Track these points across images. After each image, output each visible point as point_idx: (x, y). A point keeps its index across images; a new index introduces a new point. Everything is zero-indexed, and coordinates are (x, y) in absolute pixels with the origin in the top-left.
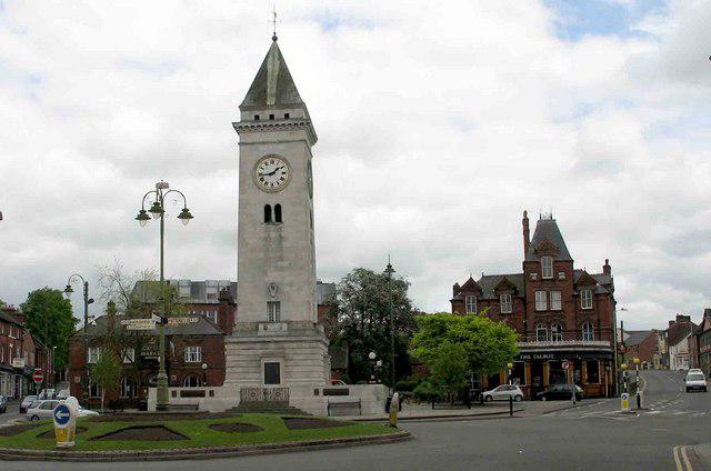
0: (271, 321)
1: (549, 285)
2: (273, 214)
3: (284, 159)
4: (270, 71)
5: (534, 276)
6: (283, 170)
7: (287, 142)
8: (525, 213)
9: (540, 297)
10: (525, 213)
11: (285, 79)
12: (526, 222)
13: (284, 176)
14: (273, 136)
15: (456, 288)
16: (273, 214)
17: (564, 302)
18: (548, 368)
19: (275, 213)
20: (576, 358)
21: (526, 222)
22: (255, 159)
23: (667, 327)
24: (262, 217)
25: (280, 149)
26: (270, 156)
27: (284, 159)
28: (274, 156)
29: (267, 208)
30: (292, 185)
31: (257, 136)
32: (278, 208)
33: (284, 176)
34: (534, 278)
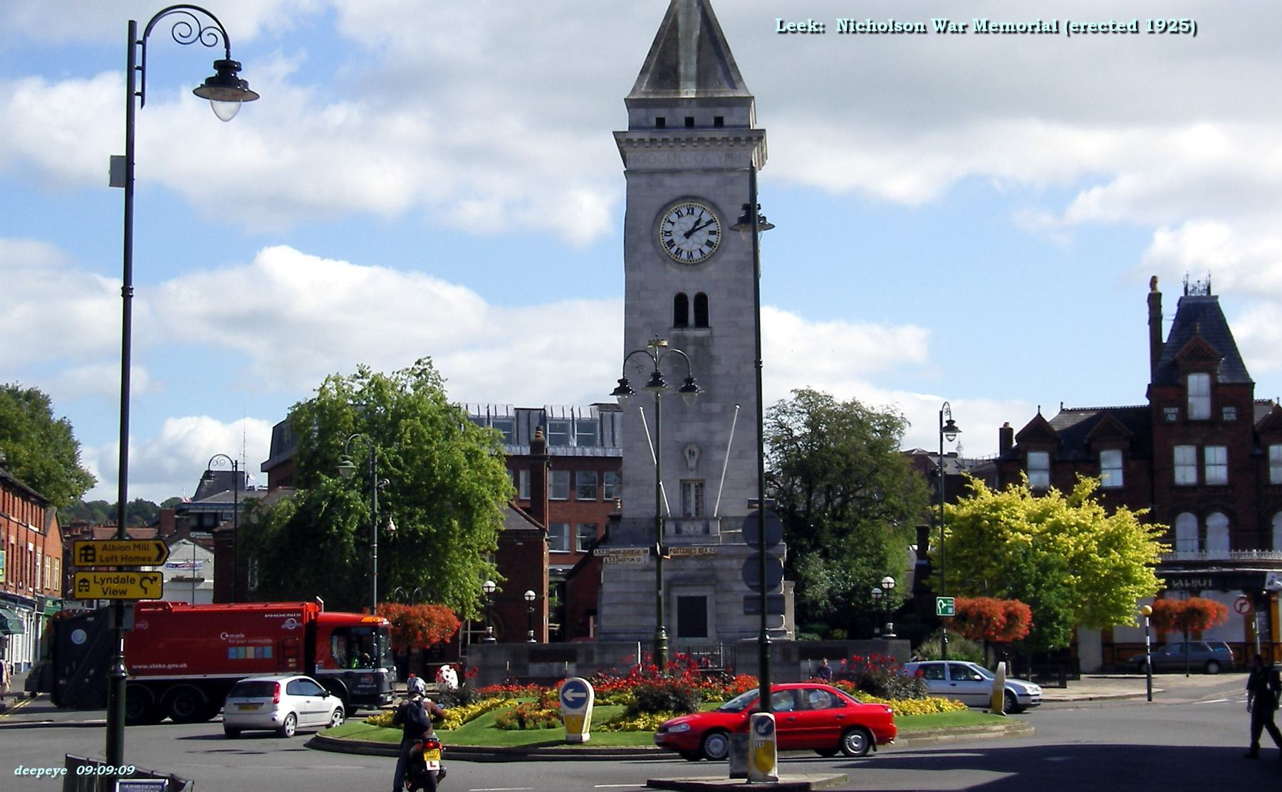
0: (687, 517)
1: (1201, 434)
2: (691, 311)
3: (714, 206)
4: (681, 27)
5: (1171, 414)
6: (712, 227)
7: (720, 170)
8: (1154, 281)
9: (1184, 454)
10: (1154, 281)
11: (713, 42)
12: (1155, 300)
13: (713, 238)
14: (688, 157)
15: (1006, 433)
16: (691, 311)
17: (1232, 464)
18: (335, 655)
19: (692, 311)
20: (342, 630)
21: (1155, 300)
22: (658, 203)
23: (451, 400)
24: (669, 317)
25: (704, 185)
26: (684, 198)
27: (714, 206)
28: (695, 198)
29: (681, 300)
30: (726, 257)
31: (661, 158)
32: (701, 300)
33: (713, 238)
34: (1172, 418)
